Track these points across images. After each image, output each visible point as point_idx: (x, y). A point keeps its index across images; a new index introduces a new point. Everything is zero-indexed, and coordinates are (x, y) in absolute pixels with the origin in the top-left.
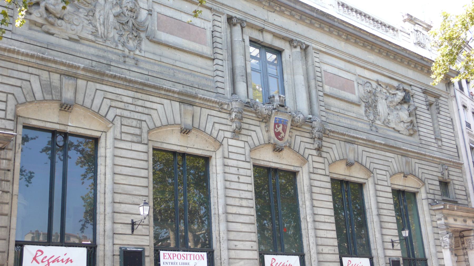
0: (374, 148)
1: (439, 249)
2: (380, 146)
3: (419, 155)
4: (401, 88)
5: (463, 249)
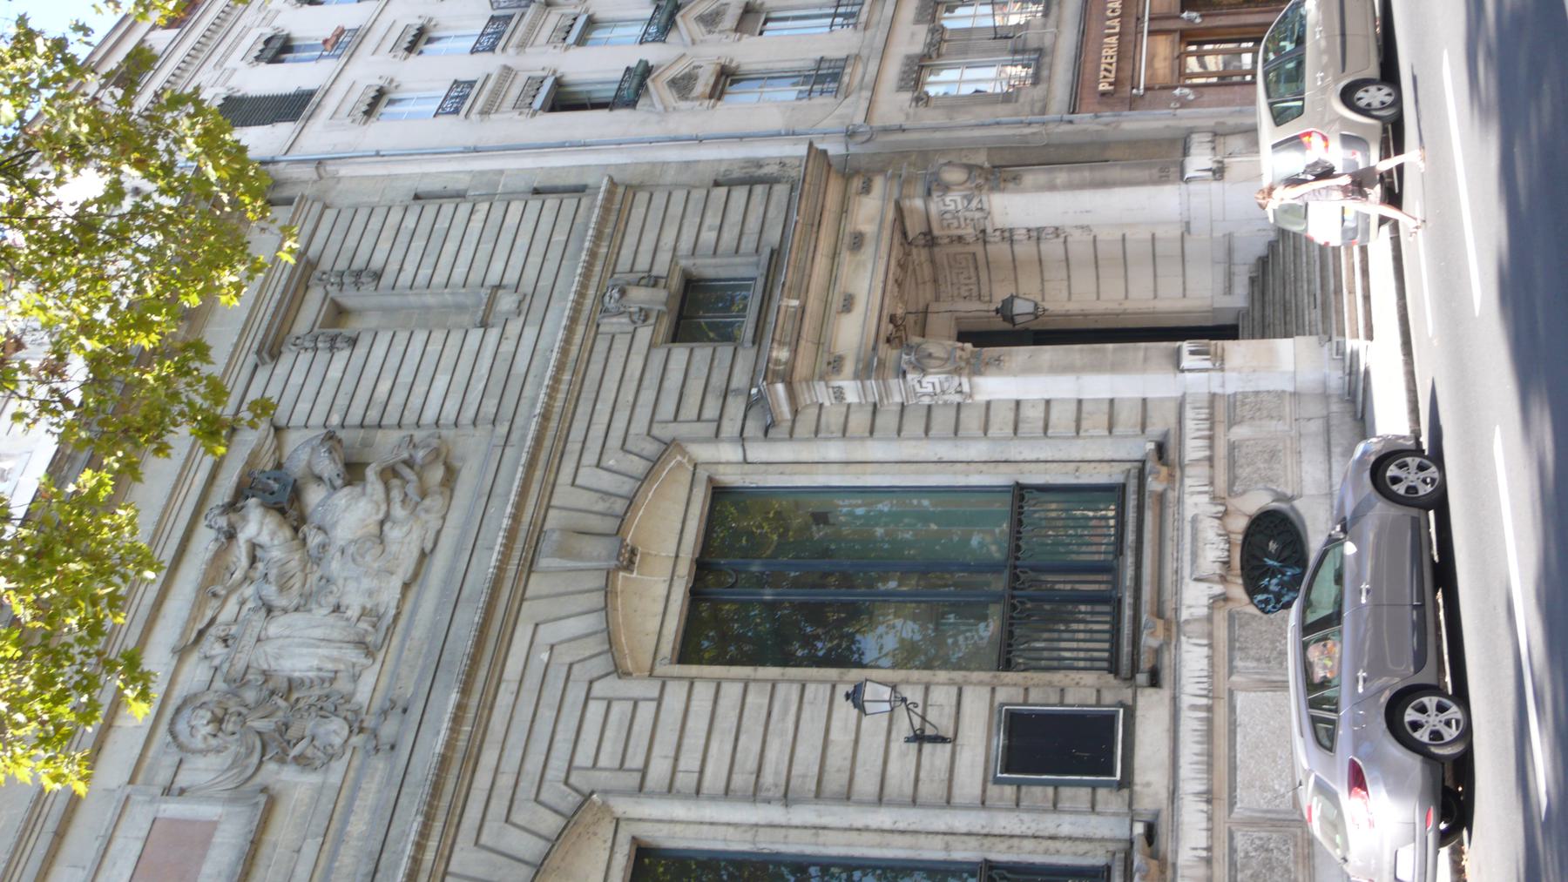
0: (472, 759)
1: (972, 421)
2: (470, 715)
3: (543, 456)
4: (222, 522)
5: (985, 242)
